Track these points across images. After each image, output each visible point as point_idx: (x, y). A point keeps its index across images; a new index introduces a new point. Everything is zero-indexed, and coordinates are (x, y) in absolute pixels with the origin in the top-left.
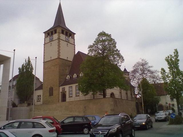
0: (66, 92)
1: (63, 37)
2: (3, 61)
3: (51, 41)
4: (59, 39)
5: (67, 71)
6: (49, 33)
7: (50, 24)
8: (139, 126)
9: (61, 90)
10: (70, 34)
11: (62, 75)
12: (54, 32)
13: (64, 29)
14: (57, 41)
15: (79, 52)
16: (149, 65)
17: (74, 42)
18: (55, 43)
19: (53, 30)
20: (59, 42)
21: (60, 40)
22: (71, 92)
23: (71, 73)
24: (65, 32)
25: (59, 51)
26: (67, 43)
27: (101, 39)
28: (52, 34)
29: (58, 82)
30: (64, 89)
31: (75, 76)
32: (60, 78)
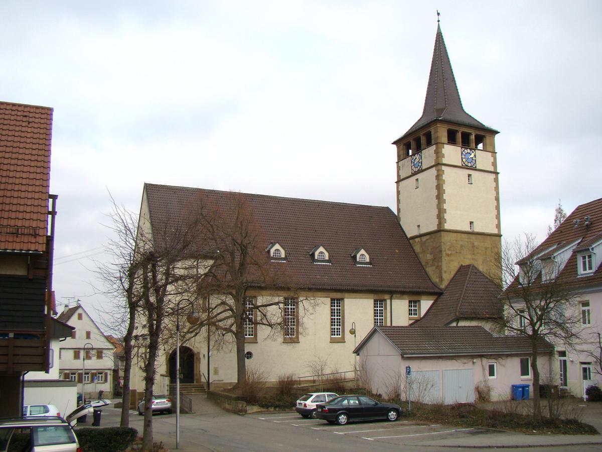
2: (566, 397)
6: (412, 143)
7: (410, 112)
8: (549, 341)
12: (423, 140)
13: (454, 128)
17: (494, 164)
21: (444, 168)
24: (459, 136)
27: (252, 235)
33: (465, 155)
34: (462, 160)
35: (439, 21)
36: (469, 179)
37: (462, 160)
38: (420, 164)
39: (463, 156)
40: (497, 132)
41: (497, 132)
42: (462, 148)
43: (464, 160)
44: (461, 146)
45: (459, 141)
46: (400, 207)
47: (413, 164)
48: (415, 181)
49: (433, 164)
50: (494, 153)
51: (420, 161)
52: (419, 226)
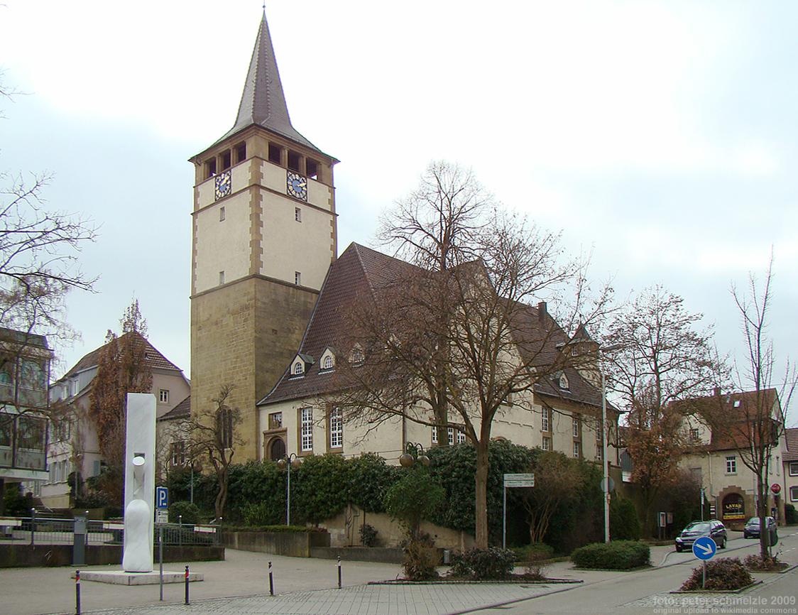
0: (286, 431)
1: (275, 176)
3: (222, 199)
4: (256, 186)
5: (297, 337)
6: (213, 162)
7: (219, 118)
9: (265, 426)
10: (308, 163)
11: (269, 354)
12: (233, 157)
13: (295, 149)
14: (248, 196)
15: (353, 248)
16: (687, 309)
17: (332, 202)
18: (240, 207)
19: (215, 154)
20: (256, 203)
21: (262, 192)
22: (308, 421)
23: (313, 346)
25: (257, 249)
26: (295, 205)
28: (227, 165)
29: (253, 388)
30: (275, 420)
31: (327, 359)
32: (259, 368)
33: (292, 182)
34: (288, 187)
35: (264, 7)
36: (296, 216)
37: (288, 187)
38: (228, 187)
39: (289, 183)
40: (336, 161)
41: (336, 161)
42: (288, 171)
43: (291, 188)
44: (287, 167)
45: (285, 156)
46: (196, 248)
47: (217, 188)
48: (219, 210)
49: (247, 186)
50: (332, 189)
51: (229, 182)
52: (222, 273)
